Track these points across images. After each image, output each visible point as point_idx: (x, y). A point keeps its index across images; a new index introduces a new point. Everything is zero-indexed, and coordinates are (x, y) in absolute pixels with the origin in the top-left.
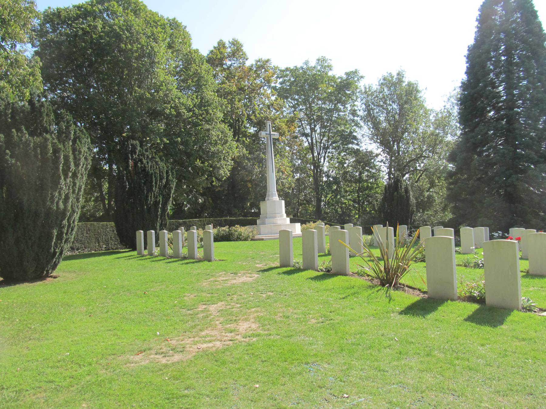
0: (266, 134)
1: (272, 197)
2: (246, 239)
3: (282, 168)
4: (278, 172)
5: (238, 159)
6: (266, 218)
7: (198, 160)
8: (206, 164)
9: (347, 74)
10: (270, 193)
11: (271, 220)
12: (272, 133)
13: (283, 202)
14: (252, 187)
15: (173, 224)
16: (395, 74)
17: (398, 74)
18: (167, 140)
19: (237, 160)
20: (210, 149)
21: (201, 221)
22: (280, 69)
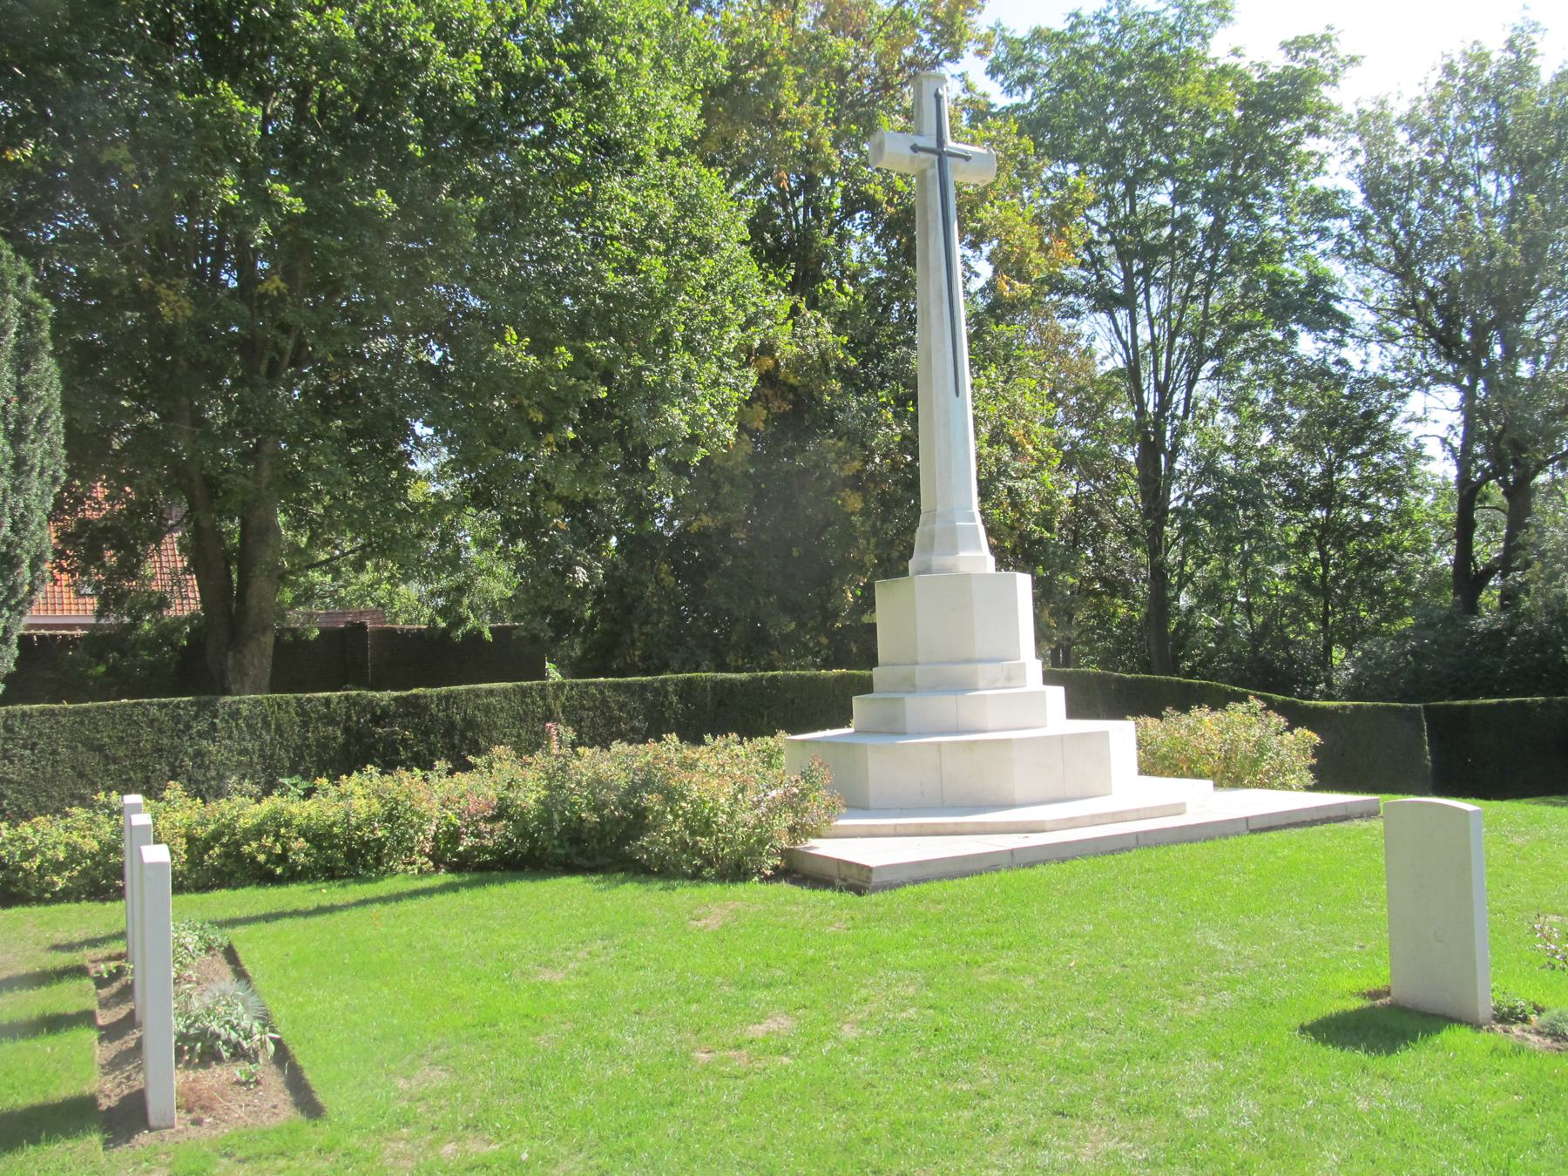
0: (915, 149)
1: (953, 549)
2: (736, 872)
3: (1014, 429)
4: (994, 440)
5: (796, 372)
6: (913, 689)
7: (511, 335)
8: (565, 355)
9: (1295, 46)
10: (938, 526)
11: (944, 706)
12: (950, 145)
13: (1023, 583)
14: (866, 512)
15: (330, 720)
16: (1498, 54)
17: (1511, 45)
18: (294, 194)
19: (792, 380)
20: (601, 280)
21: (524, 693)
22: (1007, 34)
